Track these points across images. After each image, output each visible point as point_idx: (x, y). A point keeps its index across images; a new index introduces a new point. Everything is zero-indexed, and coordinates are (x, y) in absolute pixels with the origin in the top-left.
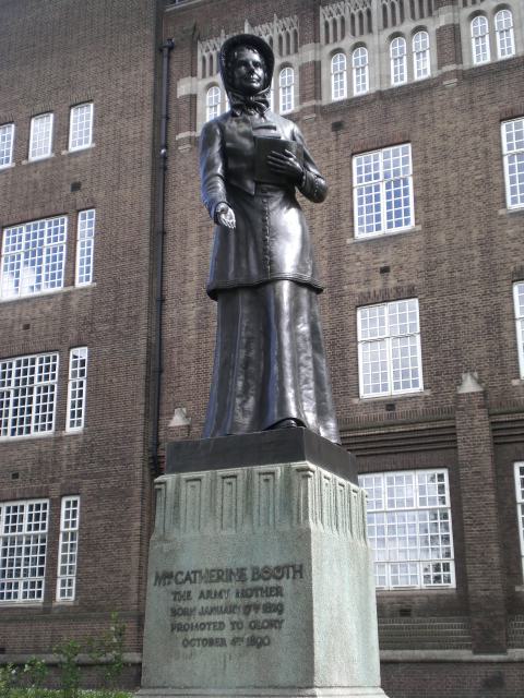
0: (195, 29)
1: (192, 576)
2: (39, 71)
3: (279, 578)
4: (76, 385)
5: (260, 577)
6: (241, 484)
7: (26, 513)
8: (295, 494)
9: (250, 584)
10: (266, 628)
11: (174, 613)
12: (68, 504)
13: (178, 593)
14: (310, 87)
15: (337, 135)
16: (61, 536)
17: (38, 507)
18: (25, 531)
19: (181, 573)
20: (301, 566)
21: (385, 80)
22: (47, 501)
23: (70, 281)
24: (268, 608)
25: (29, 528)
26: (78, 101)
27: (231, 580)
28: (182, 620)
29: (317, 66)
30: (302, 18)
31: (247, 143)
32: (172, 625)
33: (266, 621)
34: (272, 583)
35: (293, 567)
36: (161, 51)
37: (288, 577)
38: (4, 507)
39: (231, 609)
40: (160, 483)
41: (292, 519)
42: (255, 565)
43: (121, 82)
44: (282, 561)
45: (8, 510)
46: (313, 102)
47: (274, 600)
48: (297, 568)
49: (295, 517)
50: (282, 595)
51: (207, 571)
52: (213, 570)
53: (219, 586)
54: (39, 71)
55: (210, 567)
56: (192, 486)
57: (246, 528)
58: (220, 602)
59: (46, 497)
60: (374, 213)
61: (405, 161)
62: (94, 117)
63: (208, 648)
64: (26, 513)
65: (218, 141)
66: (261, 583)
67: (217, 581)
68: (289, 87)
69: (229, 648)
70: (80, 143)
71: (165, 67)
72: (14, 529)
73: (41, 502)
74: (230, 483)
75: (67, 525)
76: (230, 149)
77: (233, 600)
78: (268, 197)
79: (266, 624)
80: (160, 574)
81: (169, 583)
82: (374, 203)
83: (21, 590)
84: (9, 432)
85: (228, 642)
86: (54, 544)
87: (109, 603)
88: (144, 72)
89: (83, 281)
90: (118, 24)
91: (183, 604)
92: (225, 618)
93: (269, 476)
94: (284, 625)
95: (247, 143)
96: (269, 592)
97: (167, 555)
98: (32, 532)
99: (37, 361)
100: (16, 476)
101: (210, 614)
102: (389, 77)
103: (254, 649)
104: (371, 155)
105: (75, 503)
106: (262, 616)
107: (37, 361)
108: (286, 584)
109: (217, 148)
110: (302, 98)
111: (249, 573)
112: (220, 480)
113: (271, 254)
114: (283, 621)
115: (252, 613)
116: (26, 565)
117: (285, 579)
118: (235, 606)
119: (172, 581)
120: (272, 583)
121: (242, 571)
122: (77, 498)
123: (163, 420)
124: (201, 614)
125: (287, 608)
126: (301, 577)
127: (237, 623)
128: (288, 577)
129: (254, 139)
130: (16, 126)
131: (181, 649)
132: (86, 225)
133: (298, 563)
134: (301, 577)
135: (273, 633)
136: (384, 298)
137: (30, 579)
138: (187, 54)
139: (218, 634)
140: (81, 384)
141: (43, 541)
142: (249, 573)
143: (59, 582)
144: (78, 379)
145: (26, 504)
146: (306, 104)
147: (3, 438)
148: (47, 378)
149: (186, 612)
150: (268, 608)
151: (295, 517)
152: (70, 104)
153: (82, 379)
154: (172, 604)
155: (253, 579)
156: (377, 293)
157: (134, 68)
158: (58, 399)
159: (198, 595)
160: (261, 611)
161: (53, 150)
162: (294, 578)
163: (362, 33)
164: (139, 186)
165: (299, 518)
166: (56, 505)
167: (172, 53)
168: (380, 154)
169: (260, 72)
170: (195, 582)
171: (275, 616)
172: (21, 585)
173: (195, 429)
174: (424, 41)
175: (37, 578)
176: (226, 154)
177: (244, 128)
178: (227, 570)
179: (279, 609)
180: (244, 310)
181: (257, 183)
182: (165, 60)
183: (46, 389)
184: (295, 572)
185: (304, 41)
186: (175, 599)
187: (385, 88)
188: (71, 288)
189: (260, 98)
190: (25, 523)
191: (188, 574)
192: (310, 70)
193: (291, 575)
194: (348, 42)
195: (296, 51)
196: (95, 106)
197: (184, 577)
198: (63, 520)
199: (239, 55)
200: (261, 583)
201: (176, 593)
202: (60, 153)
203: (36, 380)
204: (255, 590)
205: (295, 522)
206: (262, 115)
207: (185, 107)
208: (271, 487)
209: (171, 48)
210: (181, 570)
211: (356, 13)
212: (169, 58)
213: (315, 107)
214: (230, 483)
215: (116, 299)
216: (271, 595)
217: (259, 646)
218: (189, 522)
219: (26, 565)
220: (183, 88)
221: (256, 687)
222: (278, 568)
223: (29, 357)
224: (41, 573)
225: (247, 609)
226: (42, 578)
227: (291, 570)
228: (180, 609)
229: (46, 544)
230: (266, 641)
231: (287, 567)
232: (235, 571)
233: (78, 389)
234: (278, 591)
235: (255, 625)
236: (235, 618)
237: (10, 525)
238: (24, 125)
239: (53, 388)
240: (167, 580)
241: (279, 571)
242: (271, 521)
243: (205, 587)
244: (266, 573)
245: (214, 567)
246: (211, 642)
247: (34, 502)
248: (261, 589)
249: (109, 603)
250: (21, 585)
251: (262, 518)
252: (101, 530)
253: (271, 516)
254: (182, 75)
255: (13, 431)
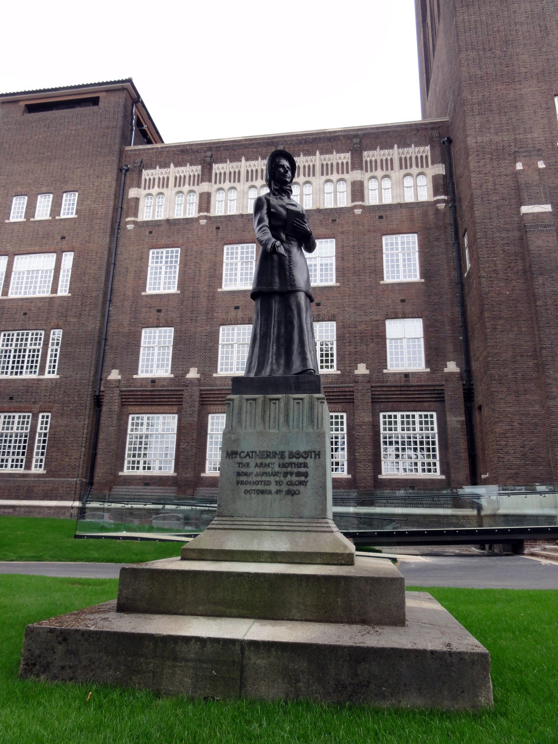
0: (142, 162)
1: (251, 454)
2: (45, 169)
3: (306, 458)
4: (54, 349)
5: (294, 457)
6: (282, 404)
7: (16, 420)
8: (316, 412)
9: (287, 460)
10: (297, 485)
11: (239, 474)
12: (43, 417)
13: (242, 463)
14: (204, 205)
15: (217, 233)
16: (37, 434)
17: (24, 417)
18: (15, 430)
19: (244, 452)
20: (319, 452)
21: (245, 209)
22: (30, 414)
23: (54, 289)
24: (298, 474)
25: (18, 429)
26: (69, 190)
27: (275, 458)
28: (244, 478)
29: (209, 195)
30: (203, 168)
31: (284, 212)
32: (237, 481)
33: (297, 481)
34: (301, 460)
35: (314, 452)
36: (121, 171)
37: (311, 458)
38: (2, 415)
39: (275, 474)
40: (229, 400)
41: (314, 425)
42: (291, 450)
43: (96, 184)
44: (308, 449)
45: (5, 417)
46: (205, 214)
47: (303, 470)
48: (317, 453)
49: (316, 424)
50: (307, 467)
51: (260, 451)
52: (264, 452)
53: (268, 461)
54: (45, 169)
55: (262, 450)
56: (274, 403)
57: (284, 429)
58: (269, 470)
59: (30, 412)
60: (233, 277)
61: (252, 252)
62: (78, 201)
63: (260, 495)
64: (16, 420)
65: (265, 207)
66: (294, 460)
67: (266, 458)
68: (150, 206)
69: (275, 496)
70: (68, 213)
71: (123, 179)
72: (7, 429)
73: (27, 414)
74: (274, 403)
75: (41, 428)
76: (273, 212)
77: (277, 469)
78: (291, 244)
79: (297, 483)
80: (230, 452)
81: (235, 458)
82: (244, 271)
83: (10, 463)
84: (9, 373)
85: (273, 492)
86: (32, 438)
87: (64, 473)
88: (109, 180)
89: (63, 291)
90: (97, 151)
91: (244, 470)
92: (272, 479)
93: (301, 401)
94: (308, 484)
95: (284, 212)
96: (299, 465)
97: (234, 441)
98: (19, 431)
99: (30, 334)
100: (11, 398)
101: (262, 476)
102: (247, 208)
103: (289, 497)
104: (235, 246)
105: (47, 417)
106: (295, 479)
107: (30, 334)
108: (310, 461)
109: (265, 211)
110: (200, 210)
111: (287, 454)
112: (268, 401)
113: (293, 276)
114: (307, 481)
115: (289, 476)
116: (4, 449)
117: (309, 458)
118: (278, 472)
119: (238, 456)
120: (301, 460)
121: (282, 454)
122: (49, 414)
123: (104, 375)
124: (256, 476)
125: (310, 474)
126: (319, 458)
127: (279, 482)
128: (311, 458)
129: (287, 210)
130: (29, 198)
131: (243, 494)
132: (68, 259)
133: (317, 450)
134: (319, 458)
135: (301, 488)
136: (236, 322)
137: (16, 457)
138: (135, 176)
139: (267, 488)
140: (56, 350)
141: (26, 436)
142: (287, 454)
143: (34, 460)
144: (55, 347)
145: (17, 415)
146: (202, 214)
147: (4, 377)
148: (35, 344)
149: (246, 474)
150: (298, 474)
151: (316, 424)
152: (64, 190)
153: (57, 347)
154: (237, 469)
155: (290, 458)
156: (232, 320)
157: (104, 177)
158: (41, 358)
159: (254, 466)
160: (294, 476)
161: (50, 215)
162: (315, 458)
163: (234, 181)
164: (101, 241)
165: (318, 426)
166: (35, 417)
167: (127, 173)
168: (240, 246)
169: (289, 173)
170: (252, 457)
171: (303, 478)
172: (10, 461)
173: (123, 382)
174: (195, 199)
175: (20, 457)
176: (269, 214)
177: (281, 202)
178: (273, 452)
179: (306, 475)
180: (275, 306)
181: (287, 236)
182: (123, 176)
183: (34, 351)
184: (316, 455)
185: (203, 181)
186: (239, 467)
187: (244, 213)
188: (54, 295)
189: (288, 188)
190: (16, 425)
191: (248, 453)
192: (205, 197)
193: (313, 456)
194: (227, 185)
195: (198, 184)
196: (79, 195)
197: (245, 454)
198: (39, 425)
199: (279, 162)
200: (294, 460)
201: (239, 464)
202: (55, 218)
203: (29, 345)
204: (291, 464)
205: (315, 427)
206: (289, 198)
207: (133, 204)
208: (301, 406)
209: (127, 170)
210: (244, 450)
211: (192, 174)
212: (125, 175)
213: (206, 216)
214: (299, 403)
215: (81, 305)
216: (300, 467)
217: (293, 495)
218: (248, 423)
219: (4, 449)
220: (133, 193)
221: (290, 517)
222: (305, 452)
223: (25, 332)
224: (23, 454)
225: (286, 474)
226: (24, 458)
227: (313, 454)
228: (243, 472)
229: (27, 438)
230: (297, 492)
231: (311, 452)
232: (278, 452)
233: (54, 353)
234: (305, 465)
235: (290, 483)
236: (277, 479)
237: (6, 426)
238: (34, 198)
239: (38, 351)
240: (234, 456)
241: (306, 454)
242: (301, 426)
243: (259, 461)
244: (298, 455)
245: (265, 450)
246: (262, 492)
247: (22, 414)
248: (294, 463)
249: (64, 473)
250: (10, 461)
251: (295, 424)
252: (63, 433)
253: (301, 423)
254: (131, 186)
255: (12, 373)
